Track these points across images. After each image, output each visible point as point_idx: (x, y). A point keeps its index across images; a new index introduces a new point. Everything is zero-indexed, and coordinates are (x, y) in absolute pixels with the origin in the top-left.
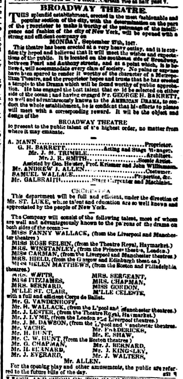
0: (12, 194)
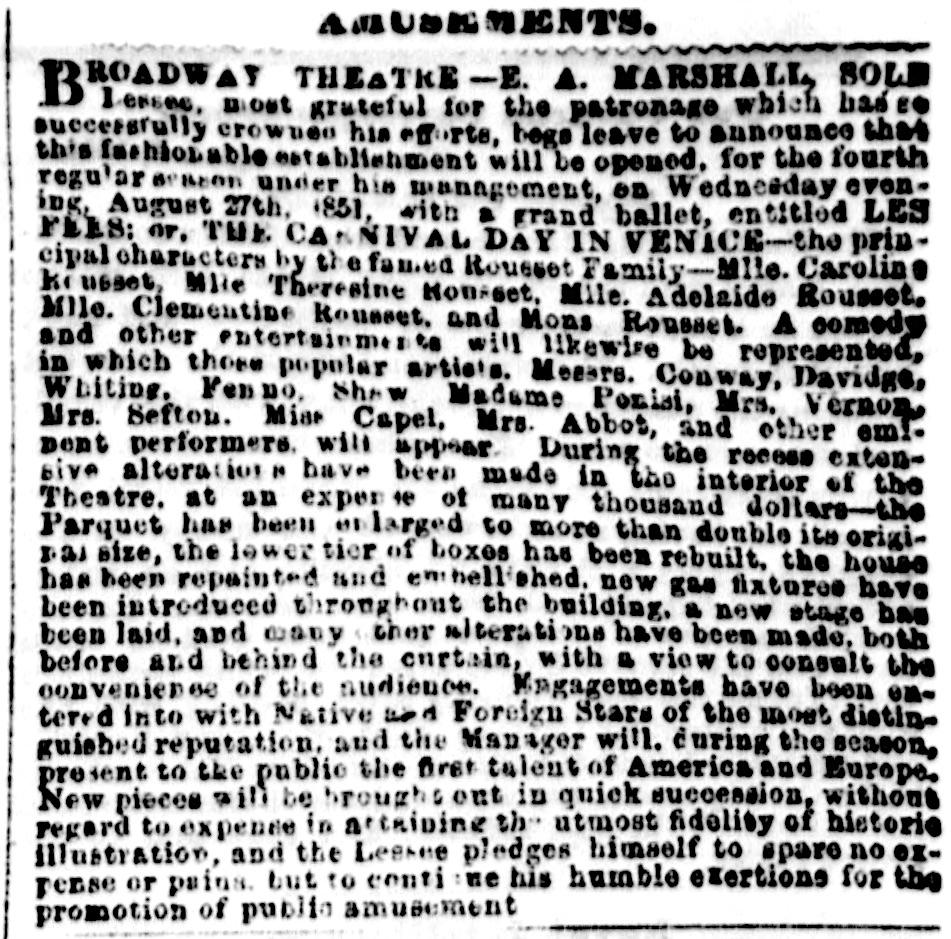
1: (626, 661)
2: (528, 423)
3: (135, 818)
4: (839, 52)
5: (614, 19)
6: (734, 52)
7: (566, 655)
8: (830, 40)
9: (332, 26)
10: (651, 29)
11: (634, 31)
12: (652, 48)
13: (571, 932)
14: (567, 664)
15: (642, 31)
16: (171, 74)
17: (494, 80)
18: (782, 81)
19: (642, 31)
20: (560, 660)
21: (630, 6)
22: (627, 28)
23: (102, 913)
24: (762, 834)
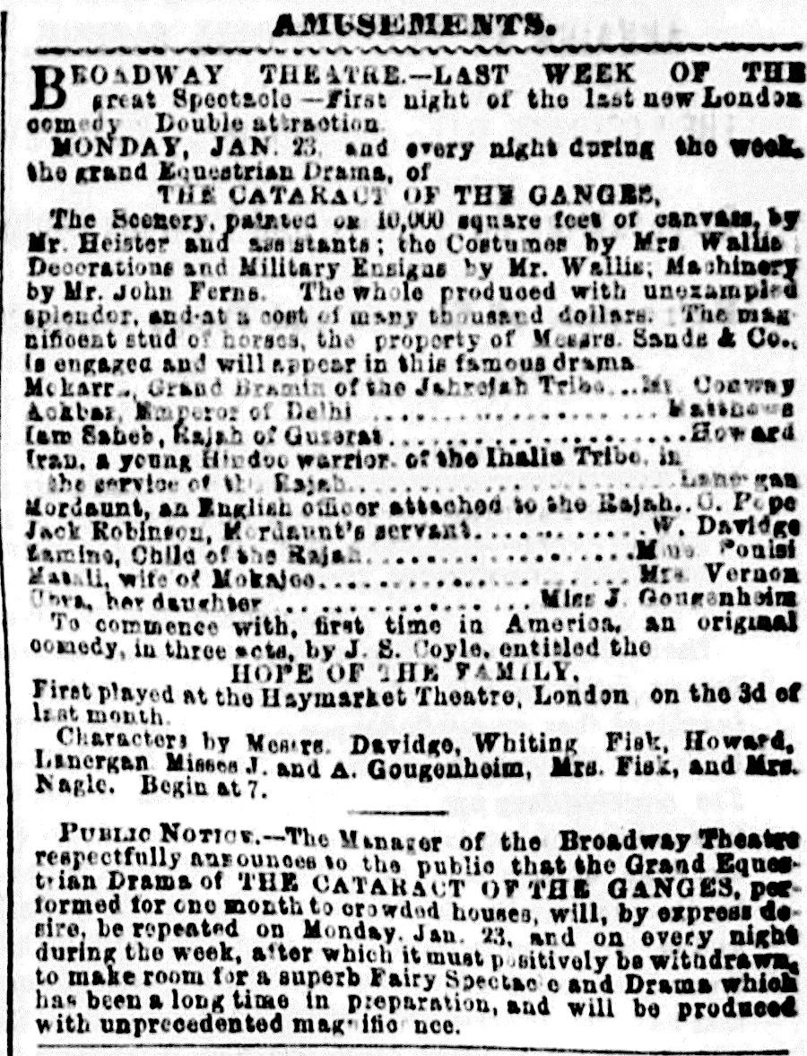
0: (34, 68)
1: (156, 1002)
2: (617, 340)
3: (126, 895)
4: (255, 54)
5: (520, 19)
6: (566, 51)
7: (60, 1023)
8: (61, 45)
9: (284, 25)
10: (552, 30)
11: (538, 32)
12: (340, 48)
13: (484, 1051)
14: (60, 1030)
15: (544, 33)
16: (143, 77)
17: (429, 77)
18: (449, 81)
19: (544, 33)
20: (55, 1027)
21: (534, 9)
22: (532, 29)
23: (239, 907)
24: (637, 924)
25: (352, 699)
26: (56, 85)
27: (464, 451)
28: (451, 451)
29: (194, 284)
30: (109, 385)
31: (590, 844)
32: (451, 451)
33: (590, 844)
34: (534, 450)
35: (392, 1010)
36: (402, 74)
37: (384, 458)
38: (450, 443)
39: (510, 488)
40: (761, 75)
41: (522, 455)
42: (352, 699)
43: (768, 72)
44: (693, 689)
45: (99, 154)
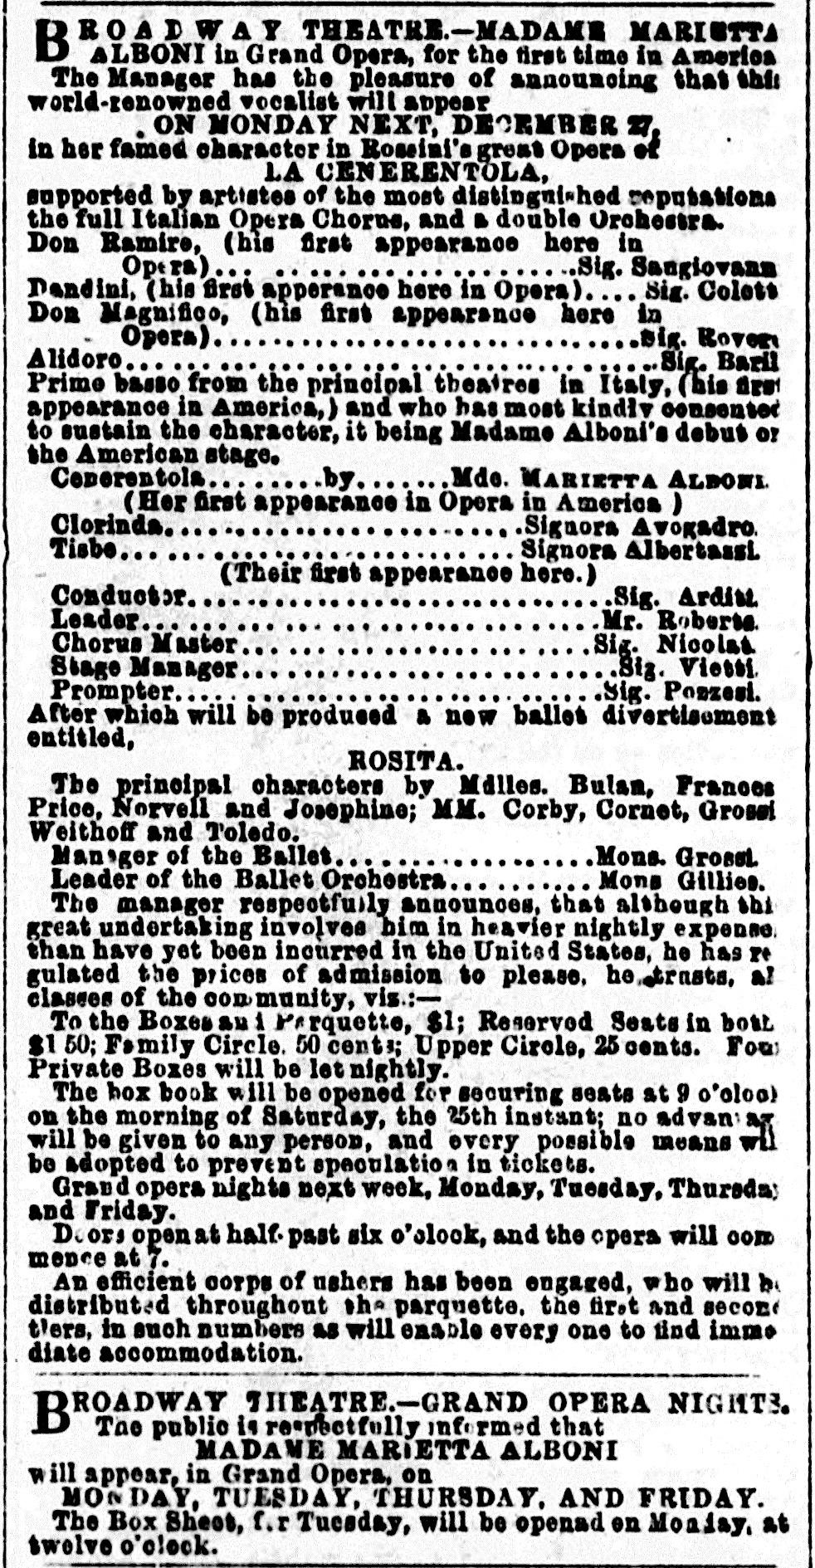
17: (469, 32)
25: (158, 1476)
26: (59, 1410)
27: (284, 376)
28: (273, 376)
29: (731, 1039)
30: (170, 689)
31: (233, 1167)
32: (273, 376)
33: (233, 1167)
34: (547, 707)
35: (47, 417)
36: (446, 29)
37: (740, 1522)
38: (272, 367)
39: (369, 555)
40: (319, 32)
41: (535, 713)
42: (158, 1476)
43: (327, 30)
44: (550, 1231)
45: (255, 131)
